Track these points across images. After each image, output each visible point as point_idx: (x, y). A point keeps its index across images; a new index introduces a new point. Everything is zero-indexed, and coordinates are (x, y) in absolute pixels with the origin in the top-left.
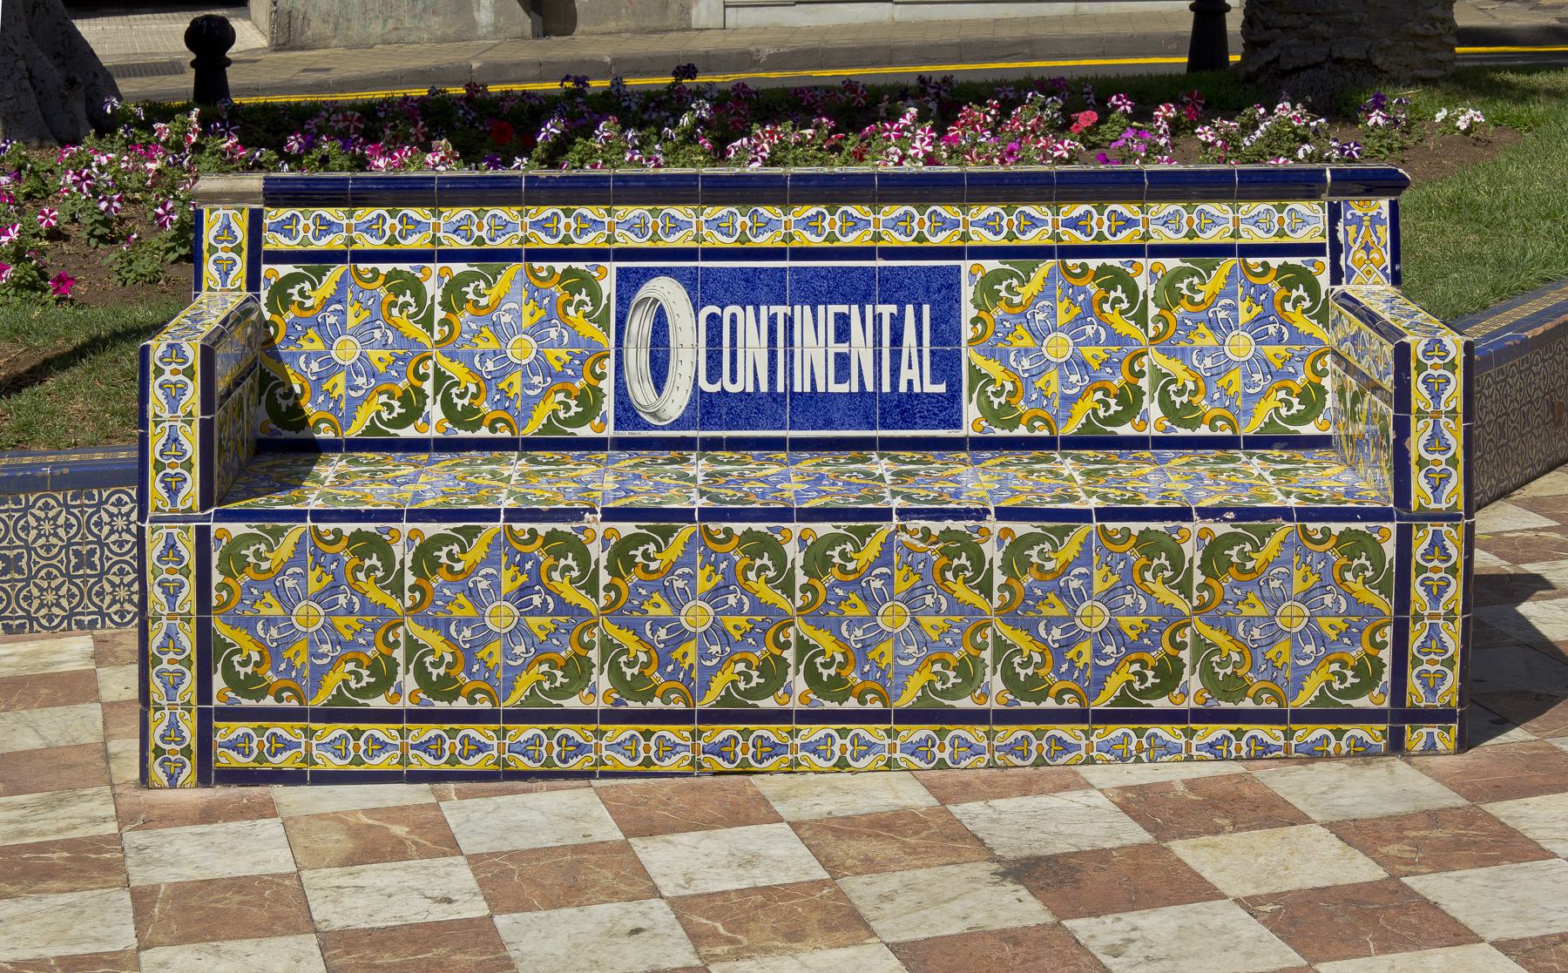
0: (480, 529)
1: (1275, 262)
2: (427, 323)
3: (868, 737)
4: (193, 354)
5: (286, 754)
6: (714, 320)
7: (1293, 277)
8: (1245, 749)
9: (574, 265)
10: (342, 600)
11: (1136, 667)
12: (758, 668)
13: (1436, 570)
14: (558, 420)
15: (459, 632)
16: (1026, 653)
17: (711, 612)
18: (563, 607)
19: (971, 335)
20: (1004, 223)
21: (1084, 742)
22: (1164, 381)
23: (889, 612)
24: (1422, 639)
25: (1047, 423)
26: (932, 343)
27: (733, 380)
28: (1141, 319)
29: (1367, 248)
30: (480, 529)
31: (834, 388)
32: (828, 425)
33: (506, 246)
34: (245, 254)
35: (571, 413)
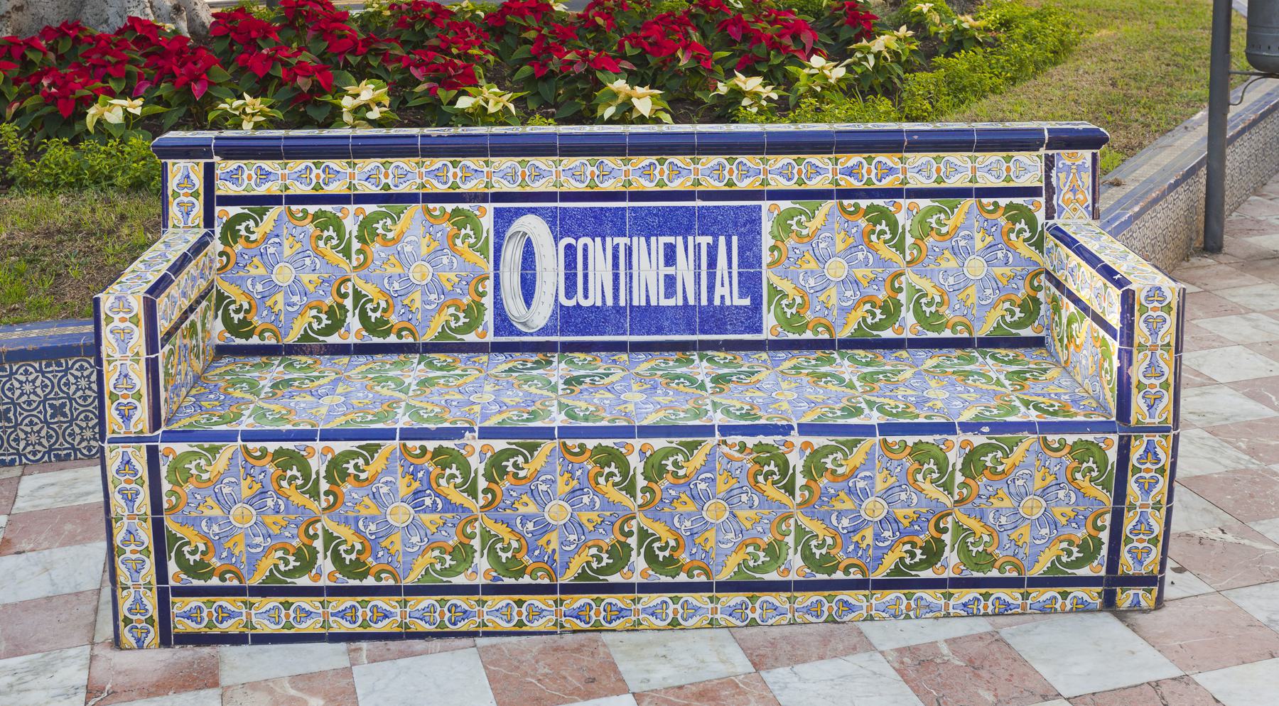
0: (380, 446)
1: (1003, 202)
2: (347, 253)
3: (695, 603)
4: (138, 306)
5: (231, 622)
6: (569, 247)
7: (1016, 214)
8: (991, 607)
9: (461, 206)
10: (270, 503)
11: (908, 547)
12: (607, 552)
13: (1148, 470)
14: (450, 329)
15: (366, 527)
16: (821, 538)
17: (569, 509)
18: (450, 506)
19: (770, 260)
20: (795, 171)
21: (865, 604)
22: (919, 296)
23: (712, 507)
24: (1134, 523)
25: (828, 329)
26: (739, 266)
27: (586, 297)
28: (900, 247)
29: (1073, 190)
30: (380, 446)
31: (664, 302)
32: (659, 331)
33: (407, 191)
34: (202, 198)
35: (460, 323)
